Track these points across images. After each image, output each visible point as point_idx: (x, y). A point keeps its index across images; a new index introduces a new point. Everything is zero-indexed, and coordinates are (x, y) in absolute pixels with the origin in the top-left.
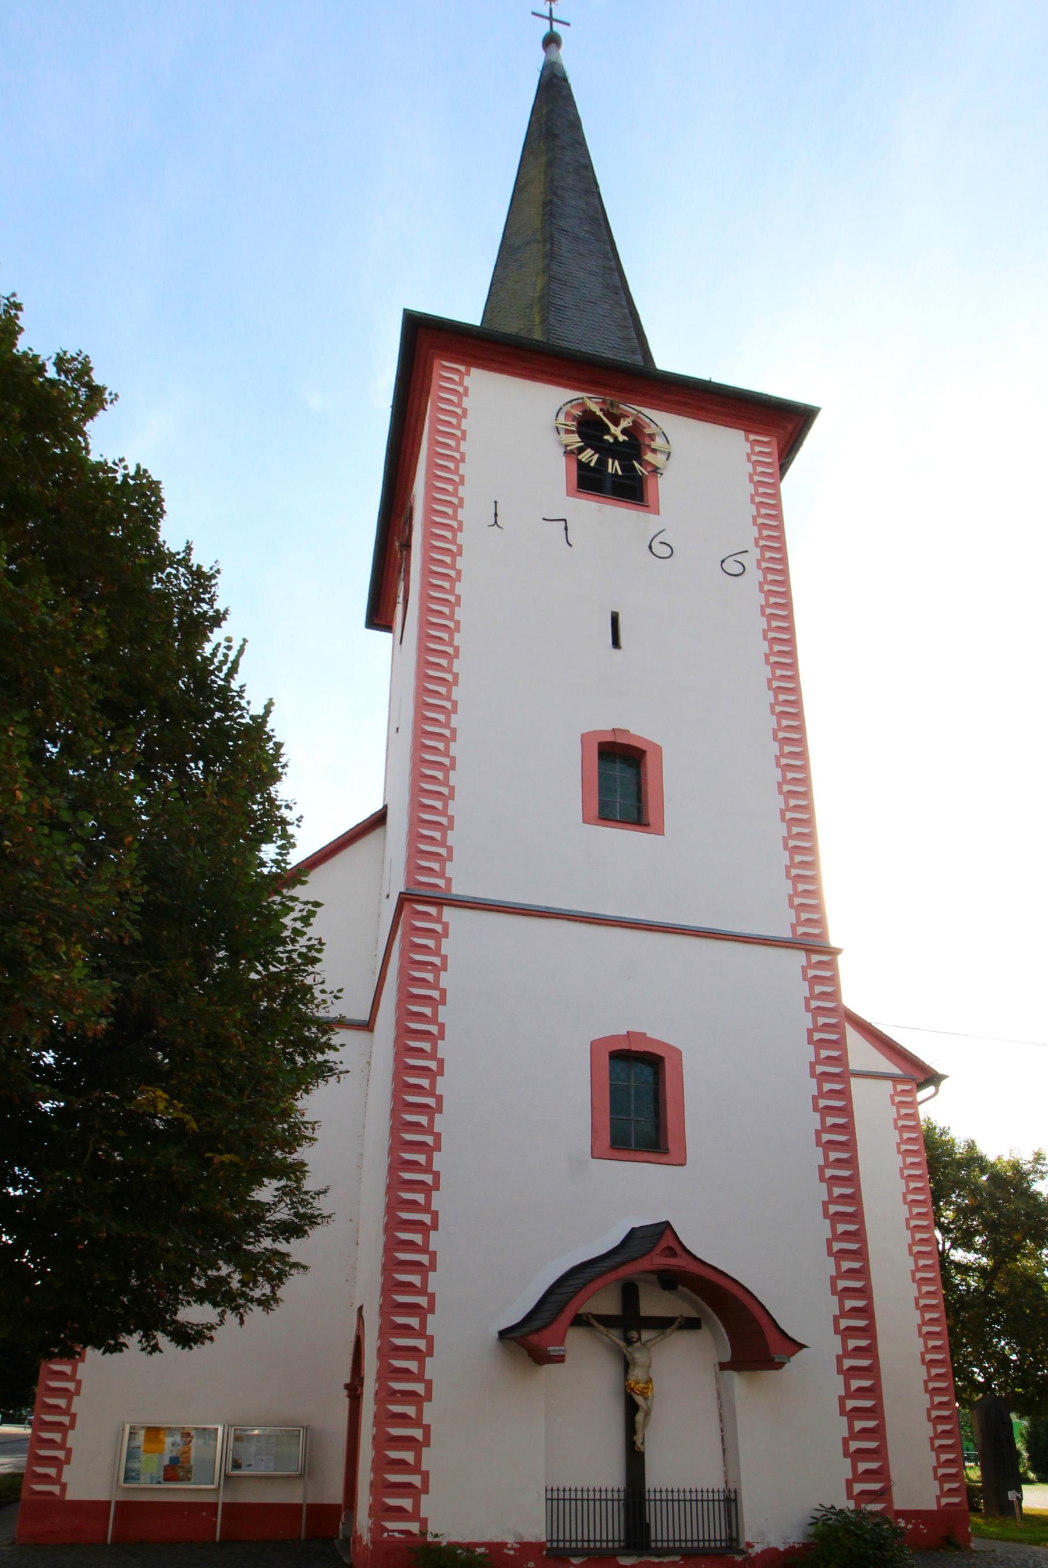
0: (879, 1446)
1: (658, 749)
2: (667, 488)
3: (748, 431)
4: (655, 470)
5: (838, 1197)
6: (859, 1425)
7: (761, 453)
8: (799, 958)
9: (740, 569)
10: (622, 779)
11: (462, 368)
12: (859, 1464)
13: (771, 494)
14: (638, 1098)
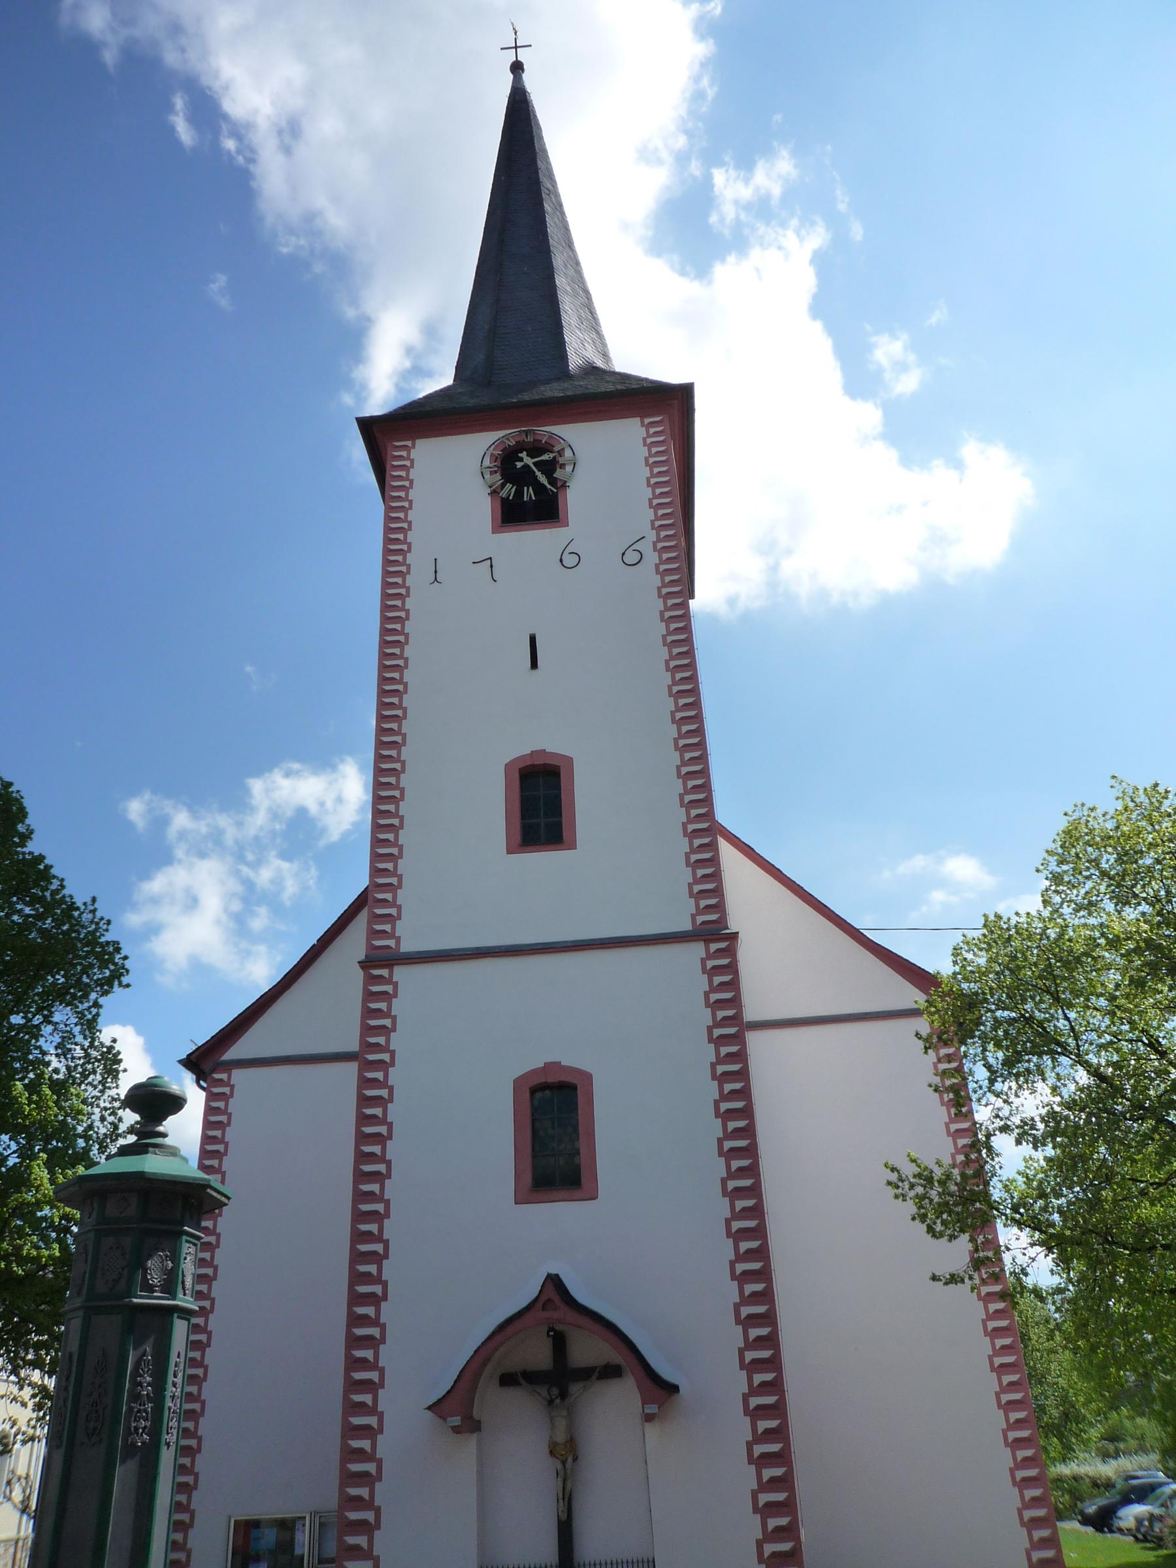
0: (777, 1401)
1: (569, 761)
2: (575, 499)
3: (642, 417)
4: (564, 486)
5: (773, 1531)
6: (728, 1087)
7: (656, 434)
8: (697, 950)
9: (637, 556)
10: (540, 804)
11: (409, 443)
12: (737, 1203)
13: (674, 558)
14: (554, 1133)
